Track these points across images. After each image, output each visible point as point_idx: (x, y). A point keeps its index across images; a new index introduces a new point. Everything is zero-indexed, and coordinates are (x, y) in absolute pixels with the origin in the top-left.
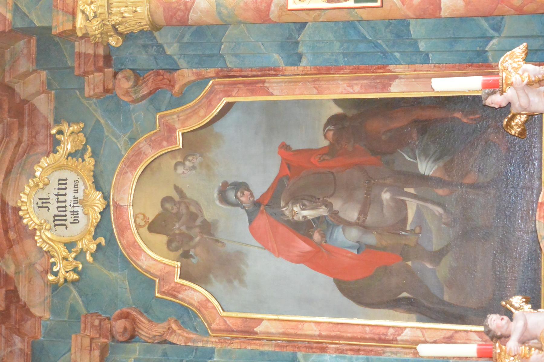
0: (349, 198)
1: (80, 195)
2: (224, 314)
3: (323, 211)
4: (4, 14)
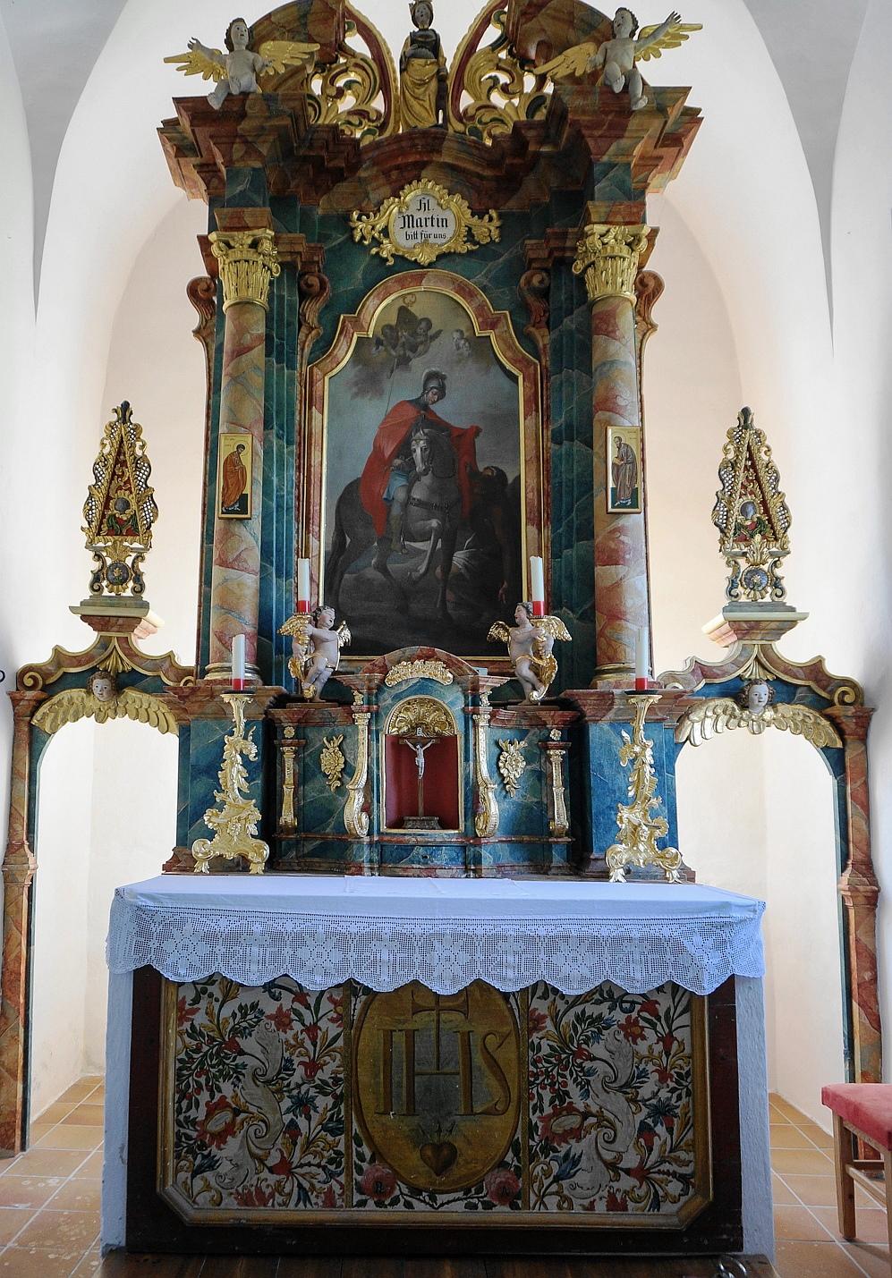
0: (432, 491)
1: (432, 240)
2: (327, 379)
3: (420, 467)
4: (607, 153)
